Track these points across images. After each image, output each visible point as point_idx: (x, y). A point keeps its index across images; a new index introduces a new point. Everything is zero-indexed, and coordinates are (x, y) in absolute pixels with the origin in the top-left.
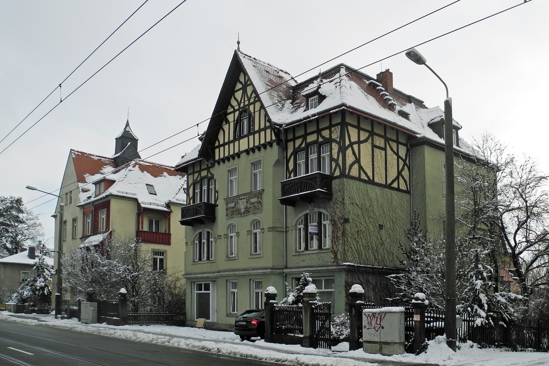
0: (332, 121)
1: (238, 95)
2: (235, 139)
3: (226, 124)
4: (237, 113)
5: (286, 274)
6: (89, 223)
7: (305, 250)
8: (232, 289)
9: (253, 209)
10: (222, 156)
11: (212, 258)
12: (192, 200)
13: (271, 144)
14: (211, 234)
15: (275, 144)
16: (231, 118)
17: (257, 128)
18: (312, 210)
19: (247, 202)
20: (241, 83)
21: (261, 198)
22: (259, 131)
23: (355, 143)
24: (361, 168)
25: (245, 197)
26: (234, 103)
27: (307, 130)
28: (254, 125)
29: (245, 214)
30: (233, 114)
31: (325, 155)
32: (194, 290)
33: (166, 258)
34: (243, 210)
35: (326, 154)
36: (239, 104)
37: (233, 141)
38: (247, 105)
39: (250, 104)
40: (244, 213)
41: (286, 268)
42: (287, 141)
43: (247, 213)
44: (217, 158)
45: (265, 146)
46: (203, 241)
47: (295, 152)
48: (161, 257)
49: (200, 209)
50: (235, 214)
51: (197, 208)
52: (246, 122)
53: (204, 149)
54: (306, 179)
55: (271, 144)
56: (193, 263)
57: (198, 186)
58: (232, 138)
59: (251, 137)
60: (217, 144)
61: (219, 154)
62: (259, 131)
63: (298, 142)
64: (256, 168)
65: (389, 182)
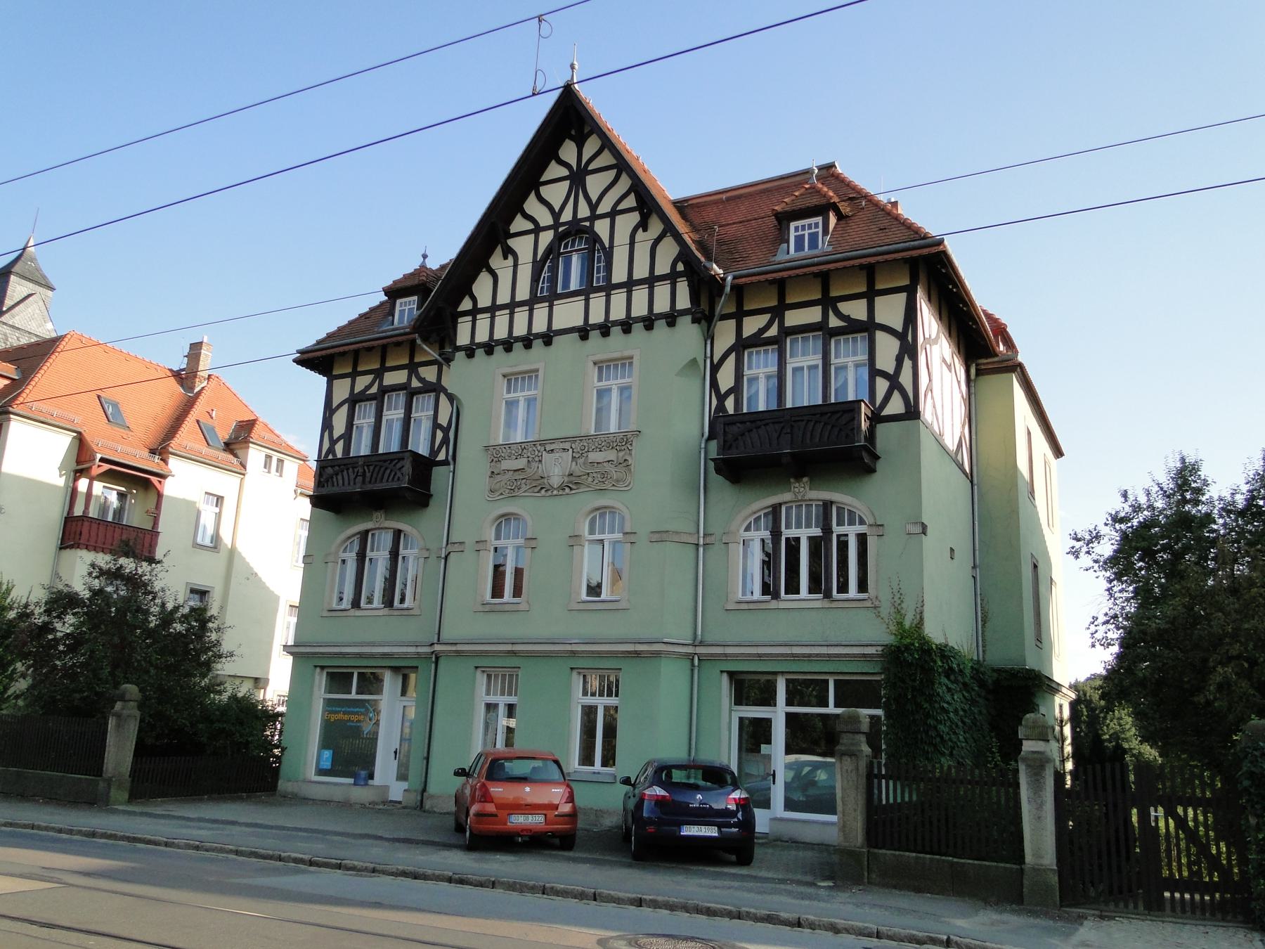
3: (505, 258)
4: (546, 238)
7: (352, 608)
11: (402, 600)
13: (671, 318)
16: (523, 247)
18: (382, 526)
27: (787, 297)
32: (320, 690)
34: (556, 481)
35: (422, 414)
36: (556, 215)
39: (594, 217)
50: (524, 488)
53: (432, 313)
54: (380, 461)
55: (671, 318)
58: (523, 293)
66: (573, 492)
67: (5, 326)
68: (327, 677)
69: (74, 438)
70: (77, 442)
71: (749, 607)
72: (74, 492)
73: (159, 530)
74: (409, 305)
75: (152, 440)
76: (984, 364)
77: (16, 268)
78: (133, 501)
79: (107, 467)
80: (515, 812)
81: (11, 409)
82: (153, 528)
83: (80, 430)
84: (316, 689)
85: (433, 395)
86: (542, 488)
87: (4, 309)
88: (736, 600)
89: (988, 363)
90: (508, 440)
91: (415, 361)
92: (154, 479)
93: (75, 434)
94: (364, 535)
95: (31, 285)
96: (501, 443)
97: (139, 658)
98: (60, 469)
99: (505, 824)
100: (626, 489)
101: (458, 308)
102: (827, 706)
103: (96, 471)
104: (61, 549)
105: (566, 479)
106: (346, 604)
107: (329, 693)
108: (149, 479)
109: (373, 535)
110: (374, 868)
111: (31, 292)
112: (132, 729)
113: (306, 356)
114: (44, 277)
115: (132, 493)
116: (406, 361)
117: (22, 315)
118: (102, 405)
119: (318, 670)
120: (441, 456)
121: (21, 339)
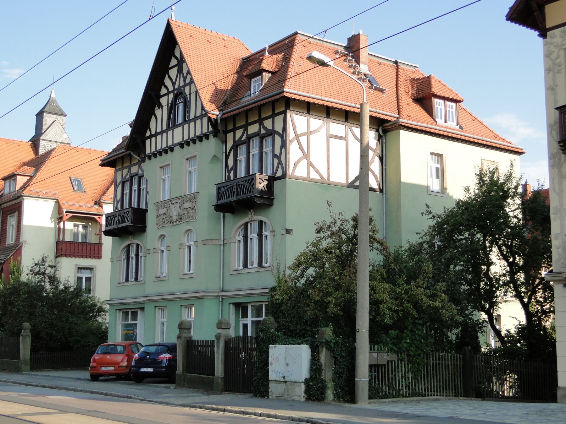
0: (275, 107)
1: (173, 72)
2: (169, 128)
3: (159, 109)
4: (171, 96)
5: (222, 299)
6: (13, 226)
7: (243, 268)
8: (161, 319)
9: (187, 217)
10: (153, 150)
12: (120, 203)
13: (207, 136)
14: (265, 223)
15: (211, 136)
16: (164, 101)
17: (192, 116)
18: (254, 217)
19: (180, 207)
20: (176, 58)
21: (196, 204)
22: (196, 119)
23: (303, 134)
24: (310, 164)
25: (177, 201)
26: (167, 82)
28: (189, 112)
29: (178, 222)
30: (167, 96)
31: (267, 149)
32: (119, 320)
33: (94, 276)
34: (175, 218)
36: (174, 84)
37: (166, 131)
38: (182, 87)
39: (185, 85)
40: (176, 221)
41: (223, 291)
42: (226, 132)
43: (179, 222)
44: (148, 151)
45: (200, 138)
46: (250, 236)
47: (236, 146)
48: (89, 275)
49: (126, 215)
51: (123, 214)
52: (181, 107)
54: (243, 181)
55: (207, 136)
56: (118, 285)
57: (127, 185)
58: (165, 128)
59: (186, 126)
60: (148, 134)
61: (151, 146)
62: (196, 119)
63: (239, 133)
64: (165, 173)
65: (351, 180)
66: (180, 223)
67: (43, 141)
68: (122, 314)
69: (56, 202)
70: (57, 204)
71: (237, 273)
72: (59, 228)
73: (102, 243)
74: (258, 82)
75: (95, 197)
76: (387, 126)
77: (46, 109)
78: (90, 229)
79: (71, 215)
80: (104, 366)
81: (22, 194)
82: (99, 242)
83: (57, 198)
84: (117, 319)
85: (271, 136)
86: (171, 222)
87: (43, 132)
88: (233, 269)
89: (389, 126)
90: (164, 199)
91: (236, 126)
92: (96, 217)
93: (56, 201)
94: (246, 225)
95: (54, 116)
96: (161, 200)
97: (38, 311)
98: (51, 219)
99: (99, 370)
100: (194, 220)
101: (146, 135)
102: (128, 321)
103: (65, 218)
104: (56, 257)
105: (178, 217)
106: (241, 267)
107: (256, 317)
108: (93, 217)
109: (251, 224)
110: (130, 397)
111: (54, 120)
112: (29, 340)
113: (104, 162)
114: (61, 110)
115: (89, 225)
116: (257, 118)
117: (51, 133)
118: (71, 183)
119: (118, 311)
120: (279, 174)
121: (52, 146)
